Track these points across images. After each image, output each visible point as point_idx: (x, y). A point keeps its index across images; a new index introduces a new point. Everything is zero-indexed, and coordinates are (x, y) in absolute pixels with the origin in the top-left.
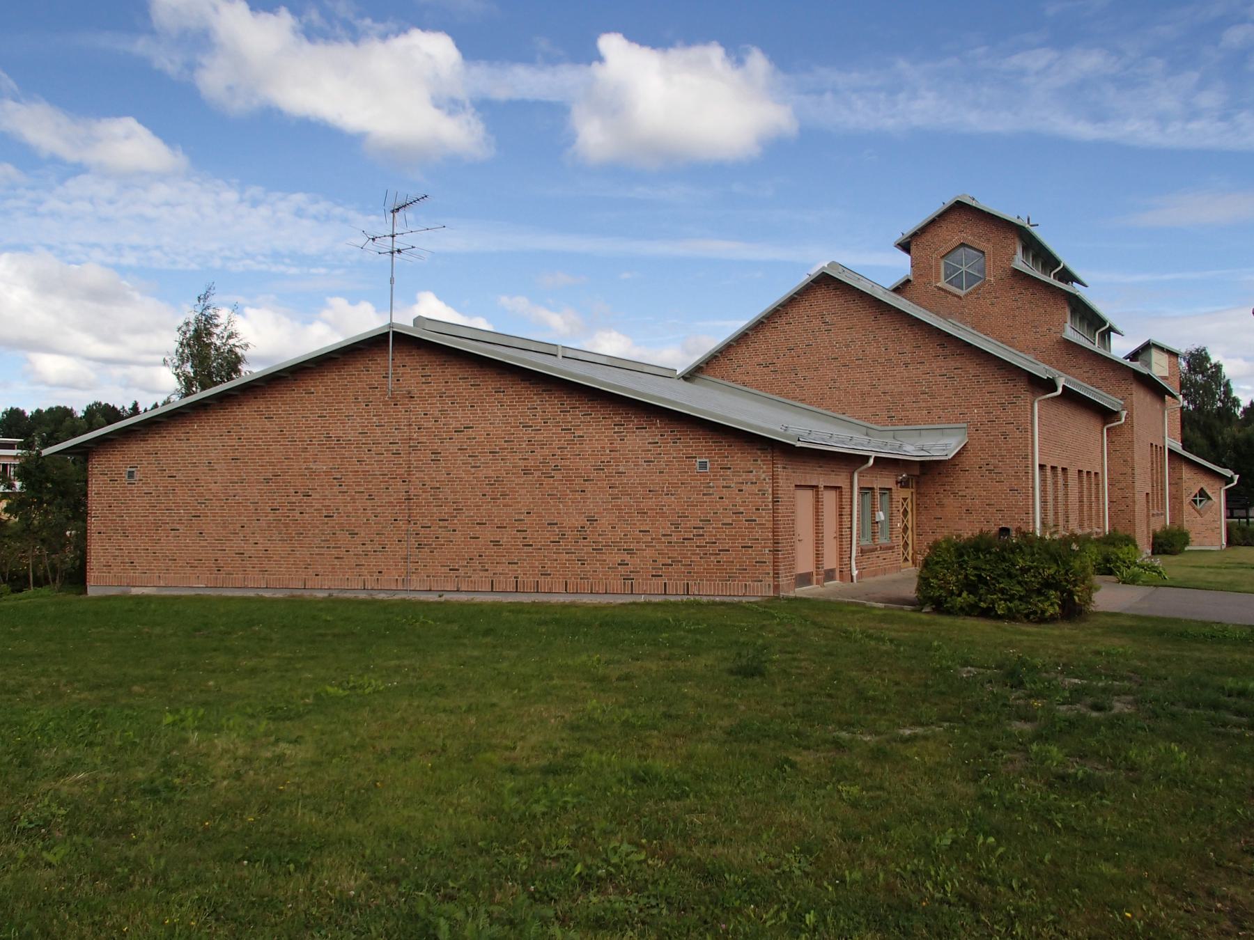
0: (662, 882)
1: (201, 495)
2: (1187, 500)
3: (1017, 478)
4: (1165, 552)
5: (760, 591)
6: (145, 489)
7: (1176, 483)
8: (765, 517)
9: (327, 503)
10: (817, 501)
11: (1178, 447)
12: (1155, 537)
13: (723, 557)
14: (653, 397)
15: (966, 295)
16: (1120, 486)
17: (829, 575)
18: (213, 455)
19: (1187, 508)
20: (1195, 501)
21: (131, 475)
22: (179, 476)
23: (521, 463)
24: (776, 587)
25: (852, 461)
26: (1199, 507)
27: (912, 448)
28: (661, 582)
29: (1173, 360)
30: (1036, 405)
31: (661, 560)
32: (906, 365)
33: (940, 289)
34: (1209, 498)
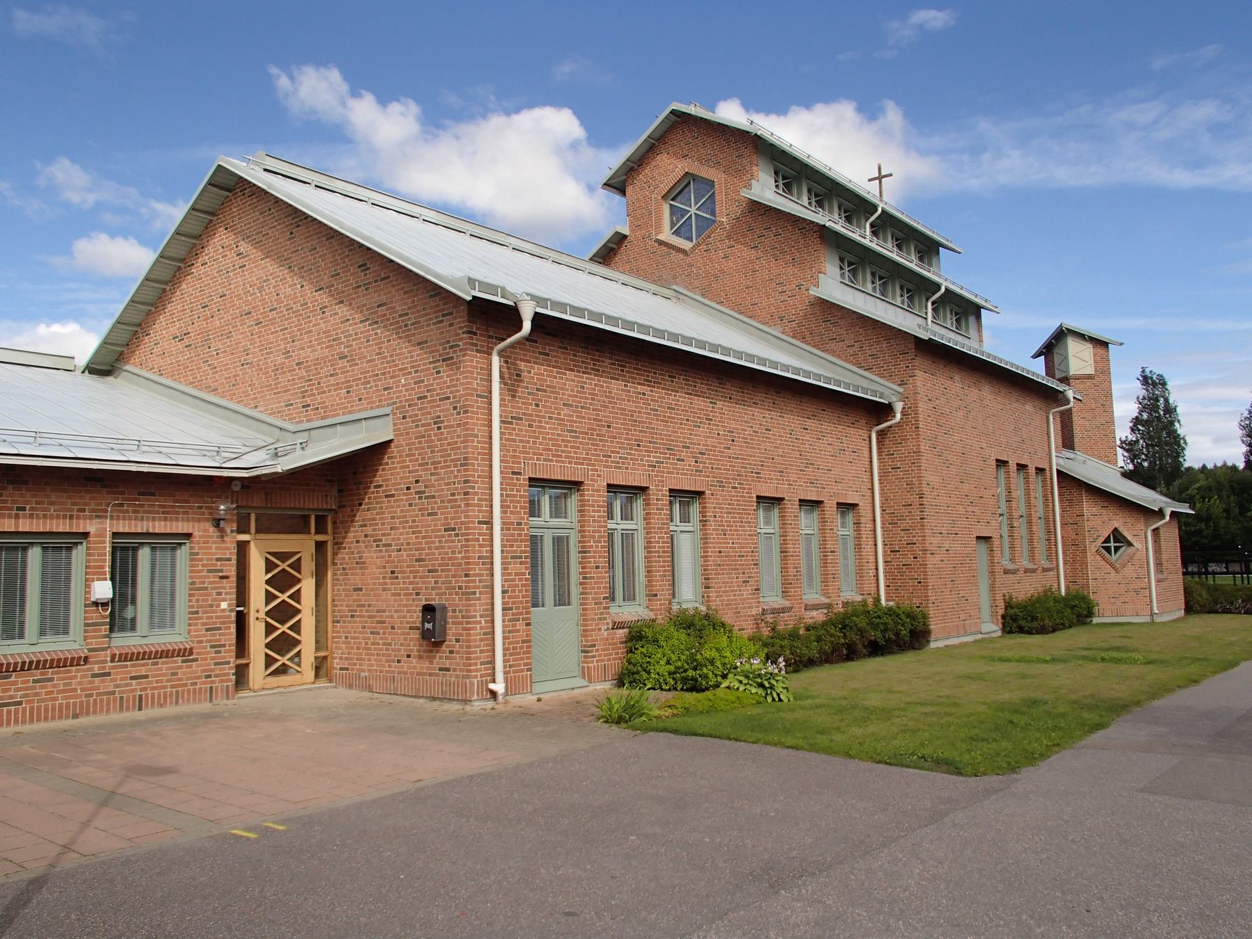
2: (1093, 546)
4: (1021, 630)
7: (1074, 523)
12: (1008, 605)
15: (694, 248)
16: (903, 525)
19: (1091, 557)
20: (1108, 549)
26: (1114, 557)
29: (1100, 351)
30: (496, 360)
33: (661, 243)
34: (1130, 544)
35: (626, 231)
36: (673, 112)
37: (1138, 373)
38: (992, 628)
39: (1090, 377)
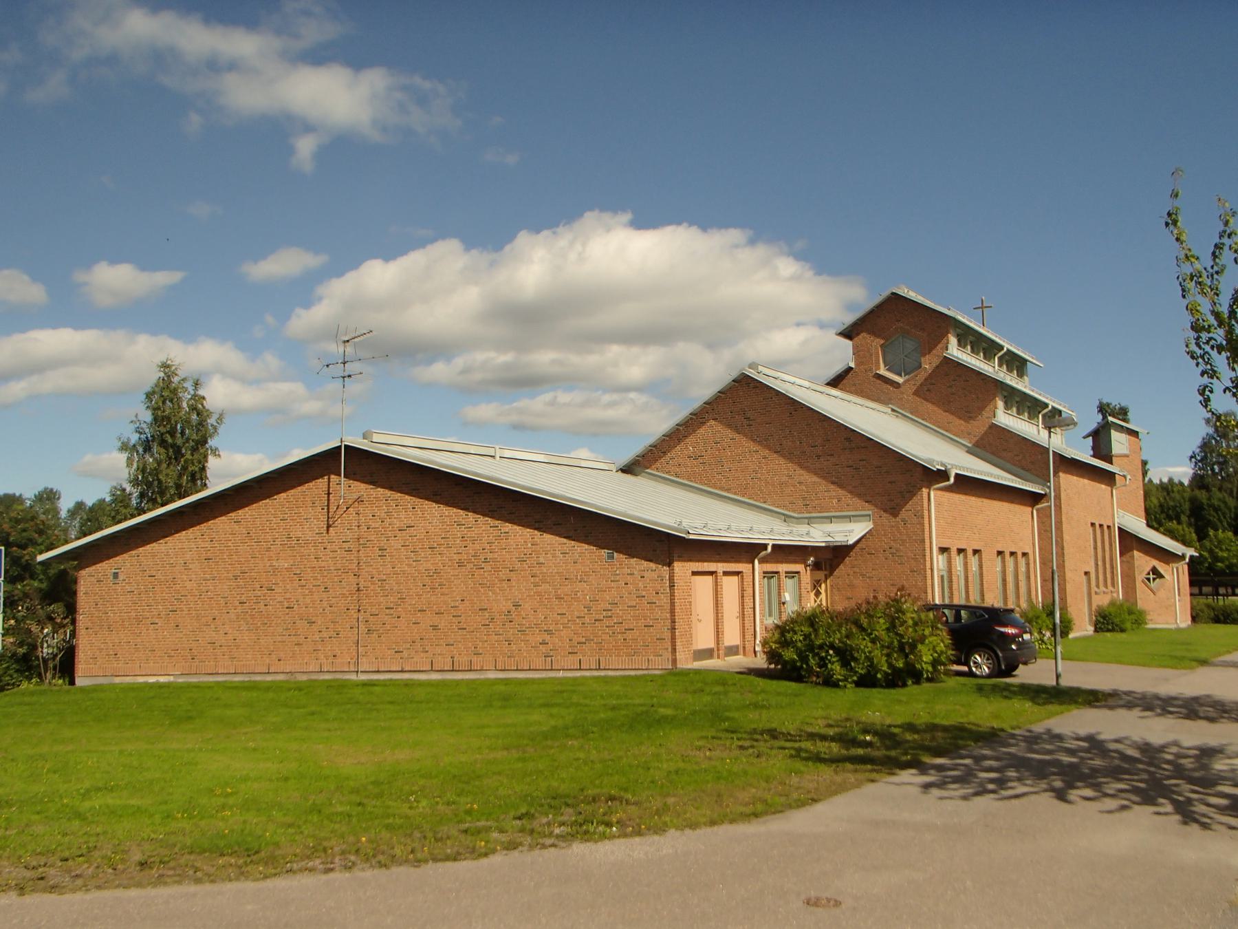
0: (346, 546)
1: (178, 592)
2: (1140, 577)
3: (915, 559)
5: (660, 664)
6: (128, 588)
8: (664, 600)
9: (288, 595)
10: (716, 584)
11: (1138, 525)
13: (629, 635)
14: (454, 468)
15: (905, 382)
17: (732, 651)
18: (188, 556)
20: (1148, 579)
21: (116, 575)
22: (159, 576)
23: (456, 557)
24: (674, 661)
25: (748, 551)
26: (1152, 585)
27: (817, 535)
28: (577, 658)
31: (576, 639)
32: (819, 457)
33: (879, 377)
34: (1161, 576)
35: (852, 365)
36: (893, 294)
37: (1097, 403)
38: (1091, 630)
39: (1127, 456)
